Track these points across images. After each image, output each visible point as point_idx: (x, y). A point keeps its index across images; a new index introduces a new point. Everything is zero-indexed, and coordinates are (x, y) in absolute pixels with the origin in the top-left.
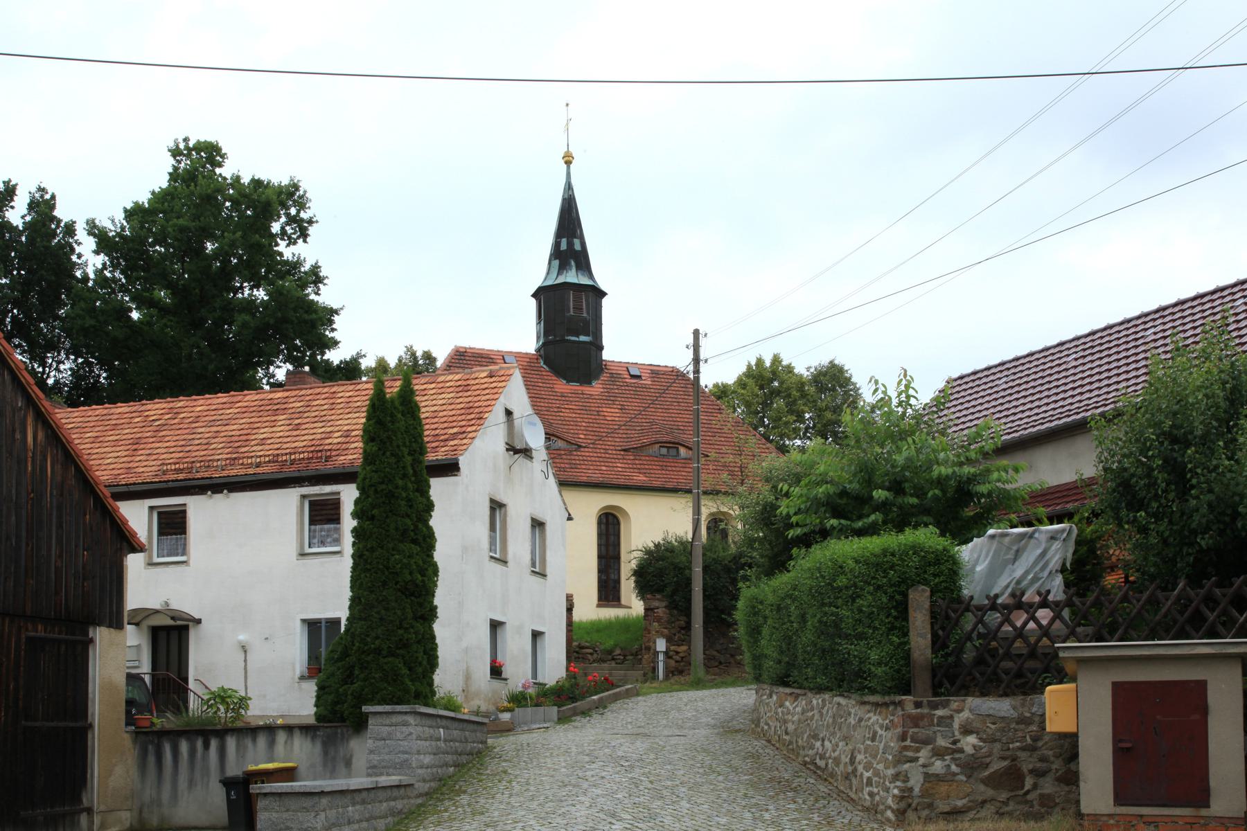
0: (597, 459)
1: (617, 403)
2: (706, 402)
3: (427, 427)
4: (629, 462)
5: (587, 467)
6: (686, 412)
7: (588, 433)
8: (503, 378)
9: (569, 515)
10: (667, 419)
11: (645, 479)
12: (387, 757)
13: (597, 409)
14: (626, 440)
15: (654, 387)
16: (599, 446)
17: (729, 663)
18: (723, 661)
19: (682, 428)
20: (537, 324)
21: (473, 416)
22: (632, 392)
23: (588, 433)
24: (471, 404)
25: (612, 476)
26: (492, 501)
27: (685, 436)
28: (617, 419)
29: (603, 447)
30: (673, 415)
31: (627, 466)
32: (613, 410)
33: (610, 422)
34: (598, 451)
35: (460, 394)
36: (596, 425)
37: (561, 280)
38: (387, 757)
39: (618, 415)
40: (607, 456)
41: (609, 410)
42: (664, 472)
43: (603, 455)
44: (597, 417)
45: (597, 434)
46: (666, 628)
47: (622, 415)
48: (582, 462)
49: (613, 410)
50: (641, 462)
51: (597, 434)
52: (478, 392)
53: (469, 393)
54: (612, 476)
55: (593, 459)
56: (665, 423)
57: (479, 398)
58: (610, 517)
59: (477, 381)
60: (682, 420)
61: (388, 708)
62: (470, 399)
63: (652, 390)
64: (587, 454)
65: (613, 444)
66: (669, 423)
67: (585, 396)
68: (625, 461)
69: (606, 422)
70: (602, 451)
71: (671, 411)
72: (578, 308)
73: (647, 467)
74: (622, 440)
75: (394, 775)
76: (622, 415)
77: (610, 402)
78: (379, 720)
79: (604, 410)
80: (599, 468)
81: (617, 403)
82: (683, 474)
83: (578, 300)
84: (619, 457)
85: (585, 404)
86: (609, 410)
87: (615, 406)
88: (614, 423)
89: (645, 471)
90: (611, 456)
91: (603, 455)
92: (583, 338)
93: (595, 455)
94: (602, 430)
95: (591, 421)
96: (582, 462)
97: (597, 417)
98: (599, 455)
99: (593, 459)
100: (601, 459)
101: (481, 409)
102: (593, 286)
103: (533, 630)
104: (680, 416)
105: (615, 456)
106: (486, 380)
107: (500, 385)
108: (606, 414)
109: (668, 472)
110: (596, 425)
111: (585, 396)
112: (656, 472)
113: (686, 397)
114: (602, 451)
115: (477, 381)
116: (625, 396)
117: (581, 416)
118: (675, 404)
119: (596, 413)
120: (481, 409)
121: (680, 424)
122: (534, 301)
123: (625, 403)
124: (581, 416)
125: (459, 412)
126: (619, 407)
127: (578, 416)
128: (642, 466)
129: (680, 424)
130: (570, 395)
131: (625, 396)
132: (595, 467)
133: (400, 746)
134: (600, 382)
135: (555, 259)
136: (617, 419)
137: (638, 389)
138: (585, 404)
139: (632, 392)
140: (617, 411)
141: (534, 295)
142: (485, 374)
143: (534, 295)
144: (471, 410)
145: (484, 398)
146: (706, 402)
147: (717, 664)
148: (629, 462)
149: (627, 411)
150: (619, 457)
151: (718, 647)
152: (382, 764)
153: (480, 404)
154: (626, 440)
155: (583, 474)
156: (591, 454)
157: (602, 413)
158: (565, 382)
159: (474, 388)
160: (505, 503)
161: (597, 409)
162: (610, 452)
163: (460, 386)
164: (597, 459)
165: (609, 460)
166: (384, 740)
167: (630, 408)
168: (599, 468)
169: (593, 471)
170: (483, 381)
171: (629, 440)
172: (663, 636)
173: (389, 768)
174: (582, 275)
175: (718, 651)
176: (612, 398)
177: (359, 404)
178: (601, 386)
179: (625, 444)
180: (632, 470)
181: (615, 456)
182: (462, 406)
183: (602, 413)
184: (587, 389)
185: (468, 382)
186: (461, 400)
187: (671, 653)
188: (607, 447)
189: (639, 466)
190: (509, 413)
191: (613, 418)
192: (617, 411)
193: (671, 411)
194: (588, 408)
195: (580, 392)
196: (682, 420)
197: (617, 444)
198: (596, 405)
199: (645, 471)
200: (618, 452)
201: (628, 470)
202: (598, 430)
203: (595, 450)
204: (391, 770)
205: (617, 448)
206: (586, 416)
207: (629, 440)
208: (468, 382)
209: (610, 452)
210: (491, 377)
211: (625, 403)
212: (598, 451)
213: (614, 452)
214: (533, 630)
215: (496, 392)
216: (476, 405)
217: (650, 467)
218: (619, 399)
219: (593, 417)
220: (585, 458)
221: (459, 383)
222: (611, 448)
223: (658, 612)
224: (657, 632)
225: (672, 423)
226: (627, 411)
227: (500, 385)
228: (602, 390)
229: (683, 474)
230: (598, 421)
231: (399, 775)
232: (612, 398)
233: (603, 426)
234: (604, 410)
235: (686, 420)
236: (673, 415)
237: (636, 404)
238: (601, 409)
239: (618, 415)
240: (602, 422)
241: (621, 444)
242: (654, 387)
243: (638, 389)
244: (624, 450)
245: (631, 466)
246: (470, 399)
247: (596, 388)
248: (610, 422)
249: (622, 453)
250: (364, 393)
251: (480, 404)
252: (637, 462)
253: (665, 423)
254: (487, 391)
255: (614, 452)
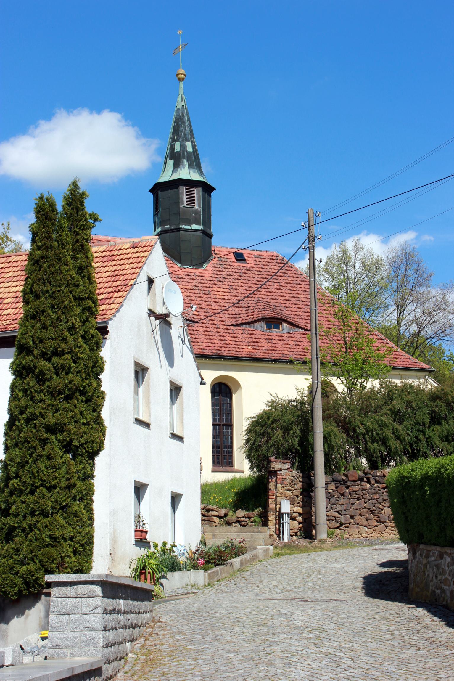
0: (210, 333)
1: (226, 283)
2: (303, 283)
3: (99, 286)
4: (238, 335)
5: (202, 340)
6: (286, 291)
7: (202, 310)
8: (145, 249)
9: (202, 379)
10: (270, 297)
11: (253, 351)
12: (71, 635)
13: (208, 289)
14: (235, 316)
15: (258, 269)
16: (211, 322)
17: (349, 523)
18: (343, 521)
19: (284, 305)
20: (154, 215)
21: (118, 283)
22: (238, 274)
23: (202, 310)
24: (116, 273)
25: (223, 349)
26: (137, 364)
27: (287, 312)
28: (226, 298)
29: (215, 322)
30: (275, 294)
31: (237, 339)
32: (222, 290)
33: (220, 301)
34: (211, 326)
35: (106, 264)
36: (208, 303)
37: (175, 176)
38: (71, 635)
39: (227, 294)
40: (219, 330)
41: (219, 290)
42: (270, 345)
43: (215, 330)
44: (209, 296)
45: (209, 311)
46: (289, 490)
47: (231, 294)
48: (197, 336)
49: (222, 290)
50: (249, 336)
51: (209, 311)
52: (123, 261)
53: (114, 262)
54: (223, 349)
55: (207, 333)
56: (268, 300)
57: (124, 267)
58: (223, 387)
59: (121, 252)
60: (283, 298)
61: (73, 577)
62: (115, 268)
63: (256, 272)
64: (201, 329)
65: (224, 319)
66: (272, 301)
67: (197, 278)
68: (235, 335)
69: (217, 300)
70: (214, 326)
71: (273, 290)
72: (191, 201)
73: (254, 340)
74: (231, 316)
75: (79, 656)
76: (231, 294)
77: (219, 283)
78: (63, 590)
79: (215, 289)
80: (212, 341)
81: (226, 283)
82: (287, 346)
83: (190, 195)
84: (230, 331)
85: (197, 285)
86: (219, 290)
87: (224, 286)
88: (224, 301)
89: (253, 344)
90: (222, 331)
91: (215, 330)
92: (194, 227)
93: (208, 329)
94: (213, 307)
95: (203, 299)
96: (197, 336)
97: (209, 296)
98: (212, 330)
99: (207, 333)
100: (214, 334)
101: (126, 277)
102: (204, 182)
103: (136, 482)
104: (282, 294)
105: (226, 331)
106: (129, 250)
107: (143, 254)
108: (216, 293)
109: (273, 345)
110: (208, 303)
111: (197, 278)
112: (263, 344)
113: (286, 278)
114: (214, 326)
115: (121, 252)
116: (232, 277)
117: (195, 295)
118: (276, 284)
119: (207, 293)
120: (126, 277)
121: (282, 301)
122: (151, 196)
123: (233, 284)
124: (195, 295)
125: (105, 279)
126: (228, 287)
127: (191, 295)
128: (251, 340)
129: (282, 301)
130: (184, 277)
131: (232, 277)
132: (209, 341)
133: (86, 621)
134: (210, 265)
135: (170, 159)
136: (226, 298)
137: (243, 271)
138: (197, 285)
139: (238, 274)
140: (226, 290)
141: (151, 191)
142: (128, 245)
143: (151, 191)
144: (117, 277)
145: (128, 266)
146: (303, 283)
147: (338, 525)
148: (238, 335)
149: (235, 291)
150: (230, 331)
151: (339, 508)
152: (66, 642)
153: (125, 272)
154: (235, 316)
155: (198, 347)
156: (205, 329)
157: (213, 293)
158: (179, 265)
159: (118, 257)
160: (147, 366)
161: (208, 289)
162: (221, 327)
163: (105, 256)
164: (210, 333)
165: (221, 334)
166: (68, 614)
167: (237, 288)
168: (212, 341)
169: (207, 345)
170: (125, 251)
171: (238, 316)
172: (287, 497)
173: (73, 647)
174: (194, 172)
175: (338, 512)
176: (221, 279)
177: (10, 274)
178: (211, 269)
179: (234, 320)
180: (241, 343)
181: (226, 331)
182: (108, 274)
183: (213, 293)
184: (197, 271)
185: (113, 253)
186: (107, 269)
187: (295, 515)
188: (219, 323)
189: (247, 340)
190: (151, 281)
191: (223, 297)
192: (226, 290)
193: (273, 290)
194: (200, 288)
195: (193, 274)
196: (283, 298)
197: (227, 320)
198: (208, 285)
199: (253, 344)
200: (229, 327)
201: (238, 343)
202: (210, 307)
203: (207, 325)
204: (75, 650)
205: (227, 323)
206: (199, 295)
207: (238, 316)
208: (113, 253)
209: (221, 327)
210: (134, 248)
211: (233, 284)
212: (211, 326)
213: (225, 327)
214: (136, 482)
215: (140, 263)
216: (121, 272)
217: (258, 340)
218: (227, 280)
219: (205, 296)
220: (199, 332)
221: (104, 254)
222: (222, 323)
223: (280, 474)
224: (281, 494)
225: (275, 301)
226: (235, 291)
227: (143, 254)
228: (212, 272)
229: (287, 346)
230: (210, 300)
231: (85, 655)
232: (221, 279)
233: (214, 304)
234: (215, 289)
235: (287, 298)
236: (275, 294)
237: (242, 284)
238: (211, 289)
239: (227, 294)
240: (213, 300)
241: (231, 320)
242: (258, 269)
243: (243, 271)
244: (234, 325)
245: (240, 339)
246: (115, 268)
247: (207, 269)
248: (220, 301)
249: (232, 327)
250: (15, 264)
251: (125, 272)
252: (246, 336)
253: (268, 300)
254: (131, 261)
255: (225, 327)
